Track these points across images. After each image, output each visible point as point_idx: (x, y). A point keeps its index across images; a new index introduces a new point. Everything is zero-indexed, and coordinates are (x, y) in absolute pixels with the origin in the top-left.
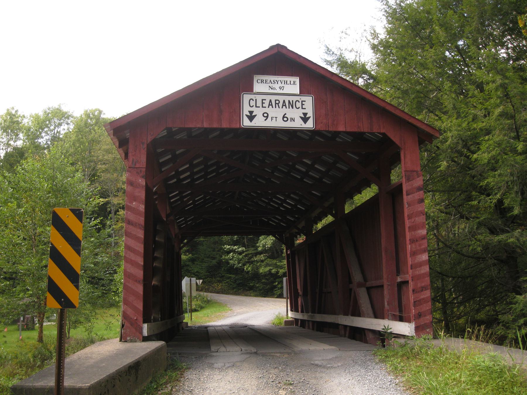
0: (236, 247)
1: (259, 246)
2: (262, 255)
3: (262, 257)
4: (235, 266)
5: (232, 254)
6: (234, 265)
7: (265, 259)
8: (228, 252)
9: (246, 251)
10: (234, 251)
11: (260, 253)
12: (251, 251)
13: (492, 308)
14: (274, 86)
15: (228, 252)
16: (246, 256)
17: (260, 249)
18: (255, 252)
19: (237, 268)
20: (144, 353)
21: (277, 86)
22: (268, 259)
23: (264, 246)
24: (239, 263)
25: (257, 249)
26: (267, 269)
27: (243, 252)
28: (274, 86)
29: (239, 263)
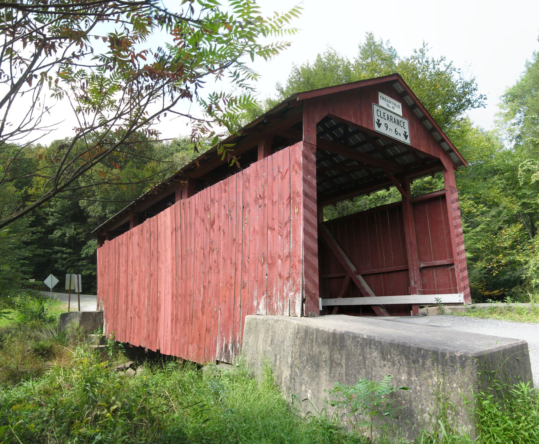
0: (64, 249)
1: (82, 254)
2: (84, 261)
3: (85, 263)
4: (482, 144)
5: (60, 254)
6: (59, 268)
7: (87, 264)
8: (57, 253)
9: (70, 257)
10: (62, 252)
11: (83, 259)
12: (74, 257)
13: (346, 212)
14: (389, 104)
15: (57, 253)
16: (70, 261)
17: (83, 256)
18: (78, 258)
19: (60, 271)
20: (488, 348)
21: (391, 105)
22: (90, 265)
23: (87, 254)
24: (62, 267)
25: (80, 256)
26: (88, 272)
27: (66, 258)
28: (389, 104)
29: (62, 267)
